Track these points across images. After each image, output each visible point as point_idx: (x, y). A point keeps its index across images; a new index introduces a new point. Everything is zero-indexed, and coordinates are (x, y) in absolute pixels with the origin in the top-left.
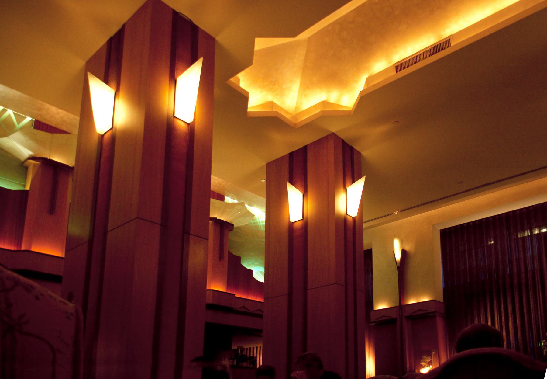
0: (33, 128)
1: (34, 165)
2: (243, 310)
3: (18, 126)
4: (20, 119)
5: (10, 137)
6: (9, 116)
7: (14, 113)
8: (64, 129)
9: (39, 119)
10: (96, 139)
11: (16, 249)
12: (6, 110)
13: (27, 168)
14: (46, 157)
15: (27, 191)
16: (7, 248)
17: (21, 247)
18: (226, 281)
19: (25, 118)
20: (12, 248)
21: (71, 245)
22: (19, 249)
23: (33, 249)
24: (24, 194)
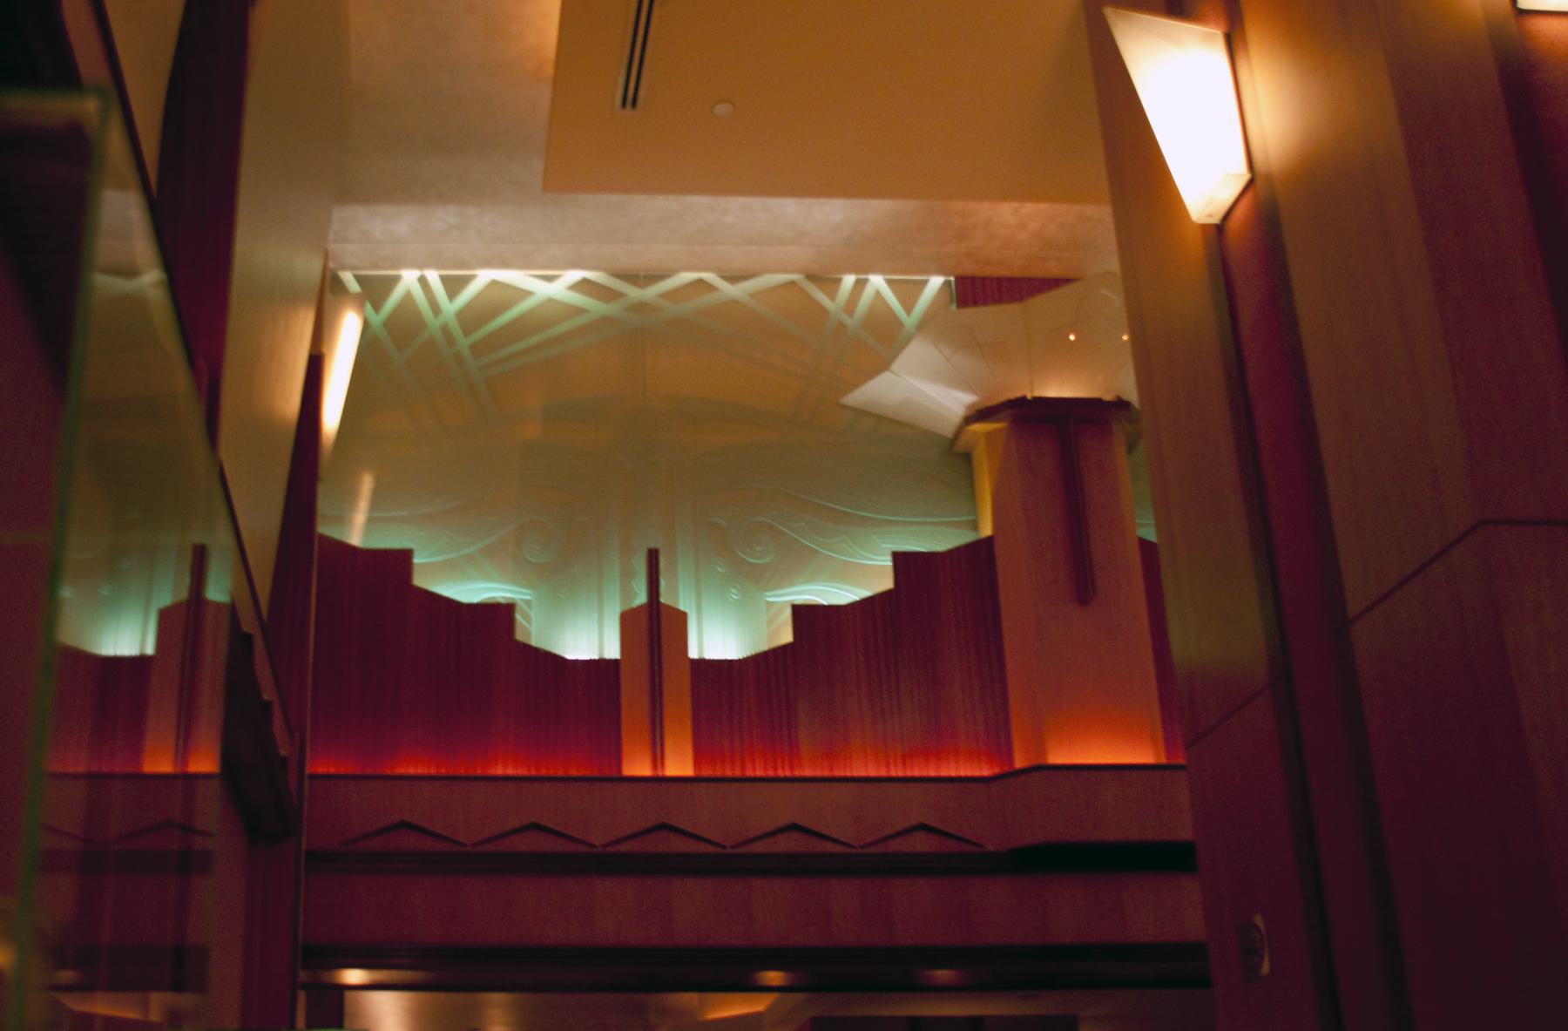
0: (954, 307)
1: (989, 436)
2: (785, 844)
3: (910, 320)
4: (907, 294)
5: (894, 367)
6: (878, 294)
7: (889, 282)
8: (1054, 269)
9: (970, 269)
10: (1195, 249)
11: (997, 770)
12: (865, 281)
13: (967, 458)
14: (1019, 394)
15: (989, 539)
16: (969, 773)
17: (1011, 762)
18: (1160, 735)
19: (926, 282)
20: (986, 772)
21: (1181, 703)
22: (1007, 769)
23: (1057, 757)
24: (978, 555)
